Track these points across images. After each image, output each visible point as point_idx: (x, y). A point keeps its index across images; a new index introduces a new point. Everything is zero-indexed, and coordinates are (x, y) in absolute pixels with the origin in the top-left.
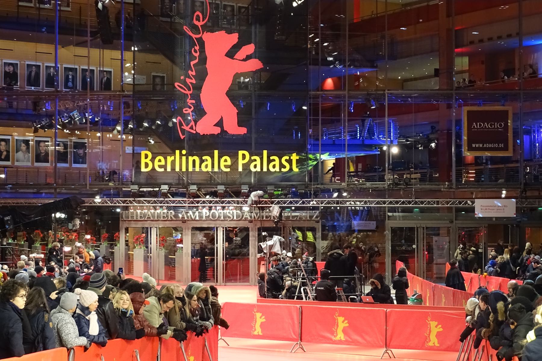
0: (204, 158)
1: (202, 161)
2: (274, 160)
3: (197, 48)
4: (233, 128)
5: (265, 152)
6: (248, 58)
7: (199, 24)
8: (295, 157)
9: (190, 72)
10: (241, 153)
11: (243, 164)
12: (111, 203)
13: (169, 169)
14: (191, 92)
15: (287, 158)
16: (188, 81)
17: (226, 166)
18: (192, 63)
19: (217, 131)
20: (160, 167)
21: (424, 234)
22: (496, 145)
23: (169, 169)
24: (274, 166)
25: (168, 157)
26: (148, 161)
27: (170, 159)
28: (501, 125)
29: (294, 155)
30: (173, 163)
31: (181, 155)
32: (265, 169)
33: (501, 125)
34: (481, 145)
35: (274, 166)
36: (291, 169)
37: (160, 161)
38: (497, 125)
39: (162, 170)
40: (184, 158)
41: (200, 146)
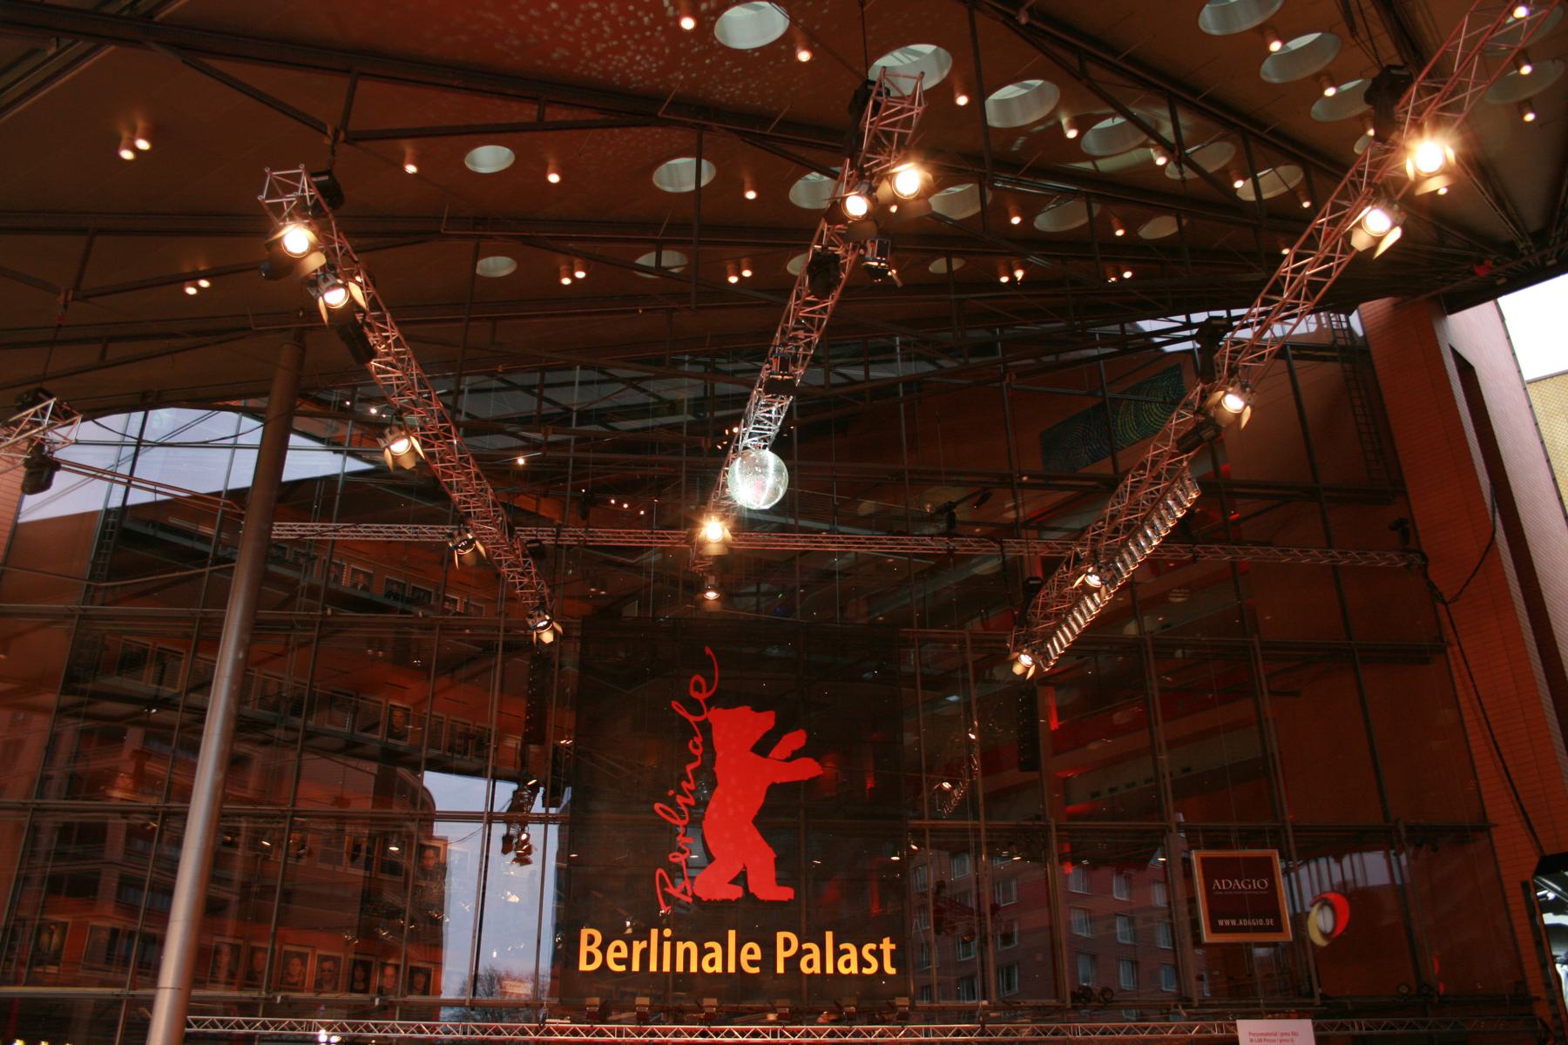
0: (707, 945)
1: (702, 952)
3: (698, 740)
4: (767, 887)
5: (829, 936)
6: (795, 755)
7: (701, 697)
8: (887, 946)
10: (781, 936)
11: (786, 959)
13: (636, 967)
16: (679, 799)
17: (752, 963)
18: (690, 768)
19: (736, 892)
20: (618, 961)
22: (1261, 922)
23: (636, 967)
24: (847, 964)
25: (636, 943)
26: (594, 949)
27: (638, 946)
28: (1262, 884)
29: (887, 940)
30: (645, 954)
31: (661, 939)
32: (830, 970)
33: (1262, 884)
34: (1234, 922)
35: (847, 964)
37: (617, 950)
38: (1256, 884)
39: (622, 968)
40: (667, 945)
41: (704, 922)
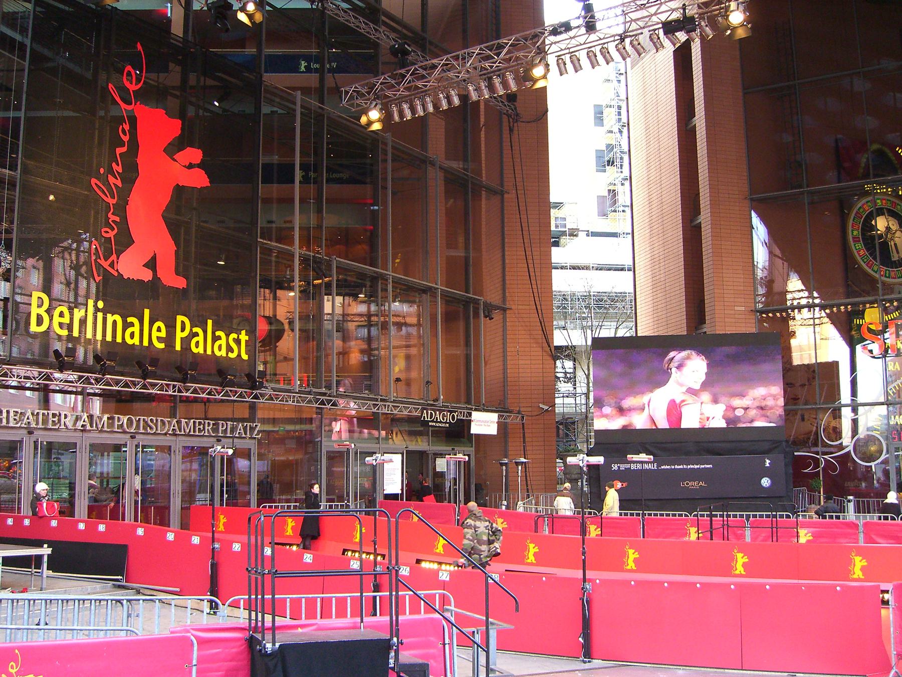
2: (219, 338)
3: (127, 127)
7: (133, 87)
16: (111, 179)
17: (61, 325)
36: (239, 355)
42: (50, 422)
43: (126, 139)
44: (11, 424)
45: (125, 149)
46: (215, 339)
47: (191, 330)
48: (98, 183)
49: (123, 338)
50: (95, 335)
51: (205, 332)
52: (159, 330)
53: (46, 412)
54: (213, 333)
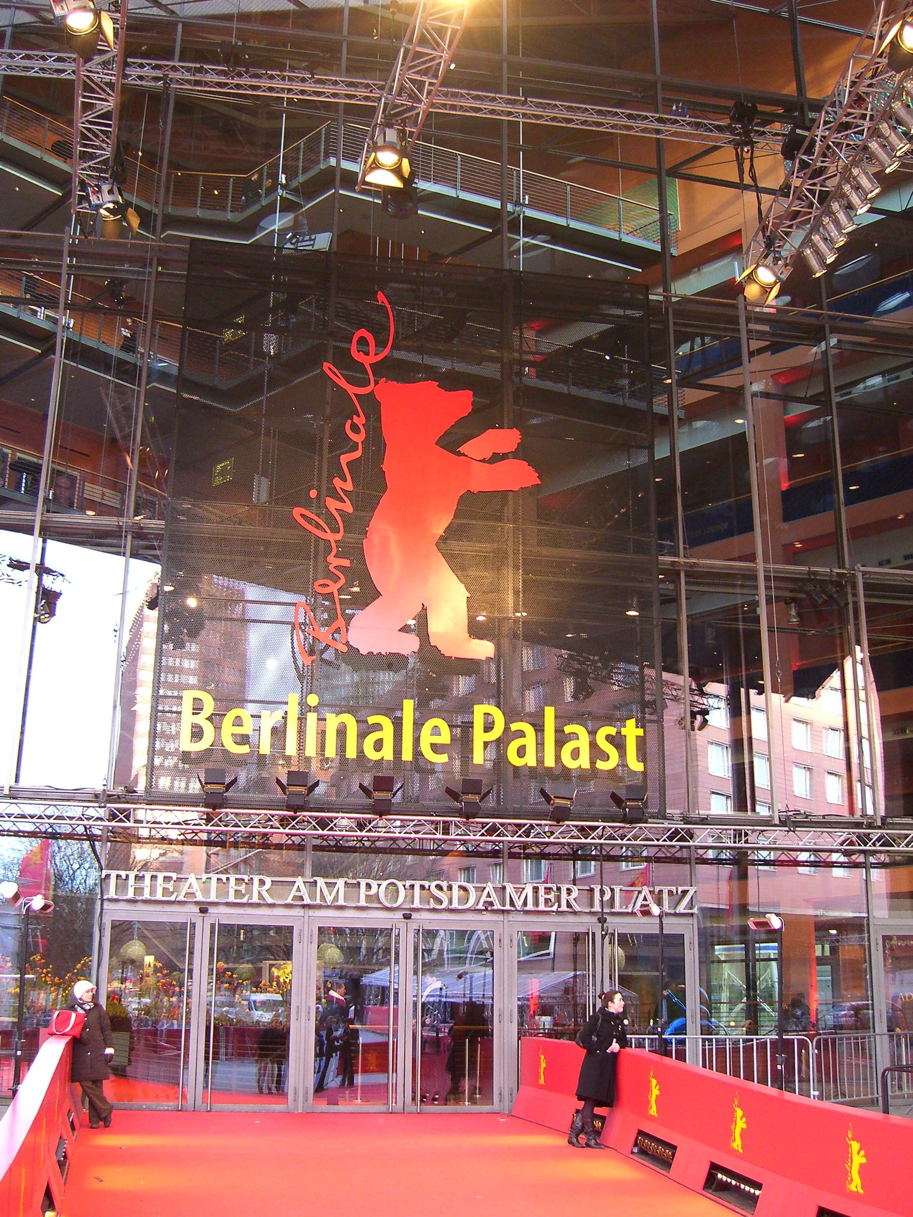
2: (378, 727)
3: (360, 421)
6: (496, 458)
7: (367, 361)
9: (337, 482)
12: (622, 840)
14: (339, 537)
15: (612, 731)
17: (435, 748)
18: (344, 459)
21: (395, 1032)
29: (631, 723)
35: (575, 754)
36: (623, 764)
42: (232, 893)
43: (358, 438)
44: (542, 907)
45: (358, 454)
46: (560, 743)
47: (507, 728)
48: (307, 513)
49: (558, 757)
50: (322, 746)
51: (539, 729)
52: (436, 731)
53: (123, 874)
54: (559, 731)
